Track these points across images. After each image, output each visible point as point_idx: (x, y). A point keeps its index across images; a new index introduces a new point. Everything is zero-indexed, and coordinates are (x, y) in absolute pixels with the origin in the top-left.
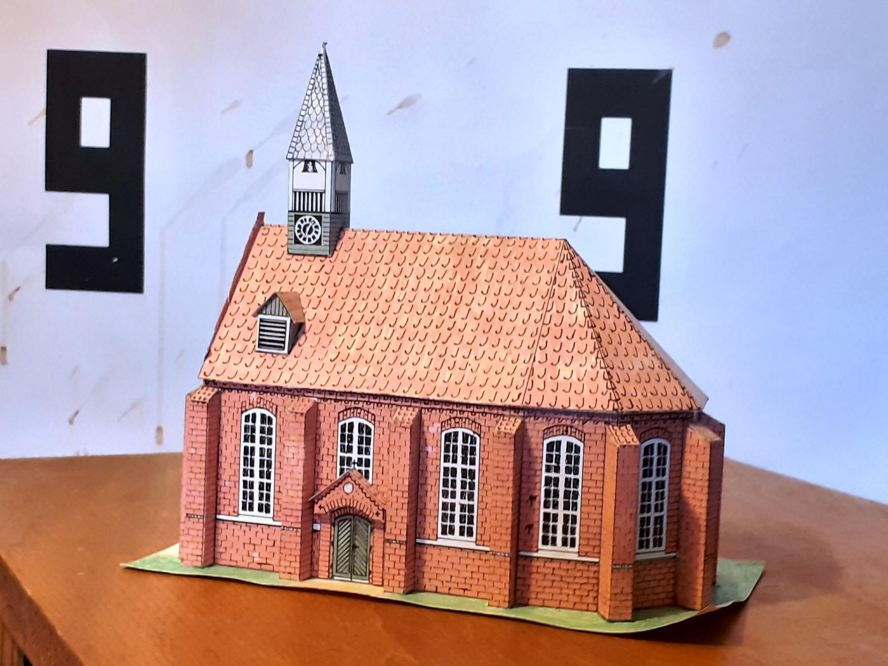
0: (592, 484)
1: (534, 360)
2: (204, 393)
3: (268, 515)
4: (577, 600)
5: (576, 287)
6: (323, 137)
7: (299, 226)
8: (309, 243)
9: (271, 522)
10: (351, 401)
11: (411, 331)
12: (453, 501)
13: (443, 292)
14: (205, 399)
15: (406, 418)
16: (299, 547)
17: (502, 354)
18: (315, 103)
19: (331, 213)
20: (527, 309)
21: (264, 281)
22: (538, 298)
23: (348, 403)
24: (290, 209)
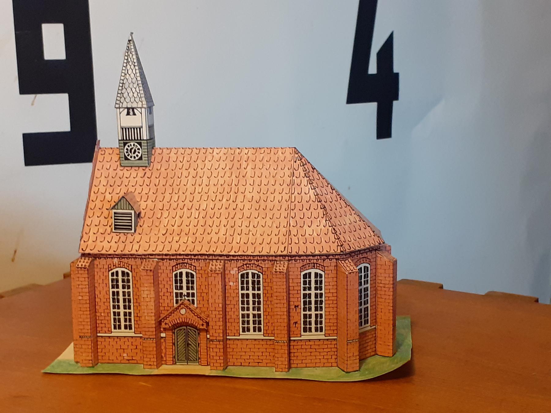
0: (330, 295)
1: (290, 225)
2: (84, 262)
3: (131, 331)
4: (325, 361)
5: (307, 177)
6: (138, 93)
7: (127, 149)
8: (135, 159)
9: (133, 335)
10: (180, 259)
11: (211, 212)
12: (248, 312)
13: (226, 186)
14: (85, 266)
15: (217, 267)
16: (155, 349)
17: (269, 223)
18: (130, 72)
19: (147, 140)
20: (279, 193)
21: (109, 185)
22: (285, 185)
23: (178, 261)
24: (120, 139)
